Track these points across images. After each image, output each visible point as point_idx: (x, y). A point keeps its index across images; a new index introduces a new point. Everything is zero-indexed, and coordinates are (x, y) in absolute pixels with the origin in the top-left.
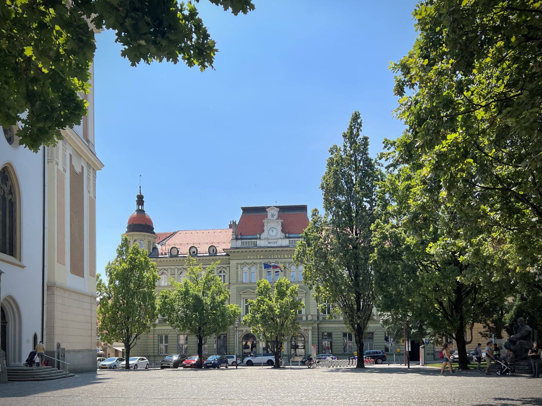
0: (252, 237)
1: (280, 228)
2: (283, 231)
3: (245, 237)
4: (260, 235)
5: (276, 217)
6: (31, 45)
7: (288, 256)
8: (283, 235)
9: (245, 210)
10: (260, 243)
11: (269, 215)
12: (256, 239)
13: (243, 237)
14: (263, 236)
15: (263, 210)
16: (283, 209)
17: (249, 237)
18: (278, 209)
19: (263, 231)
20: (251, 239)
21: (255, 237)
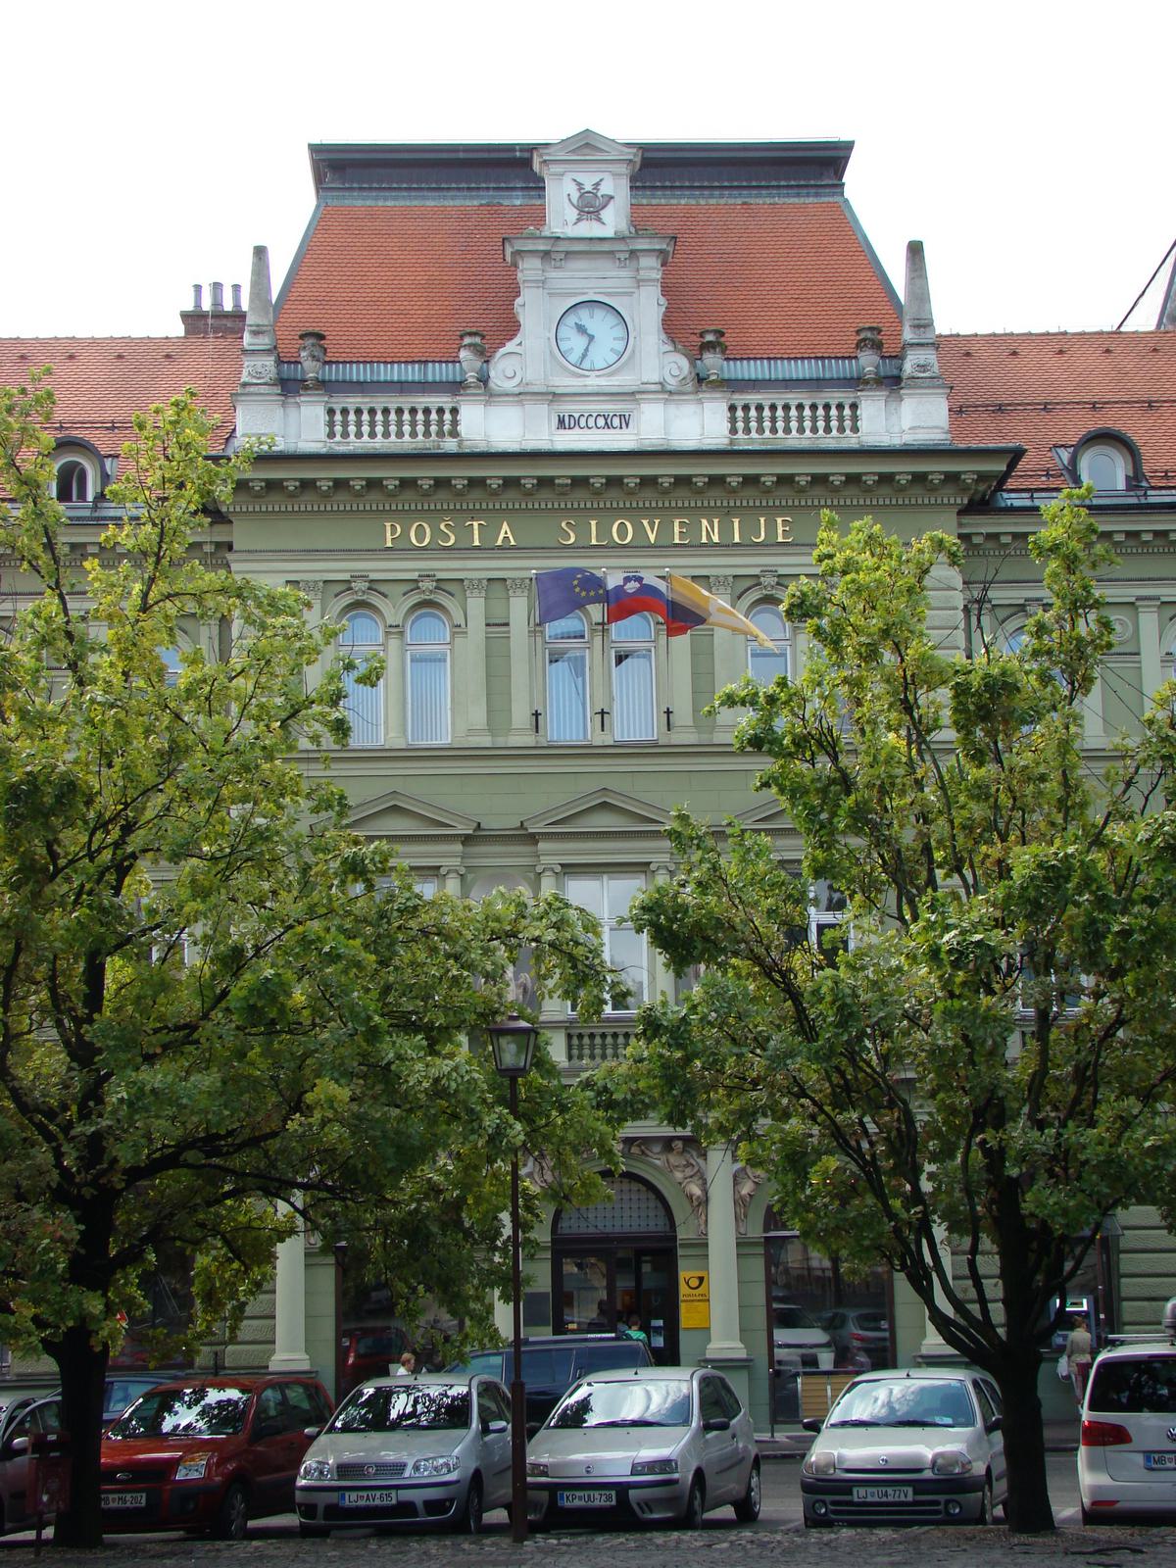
0: (412, 373)
1: (647, 308)
2: (672, 327)
3: (356, 373)
4: (485, 354)
5: (613, 221)
6: (939, 344)
7: (726, 530)
8: (678, 366)
9: (340, 167)
10: (489, 427)
11: (561, 215)
12: (456, 387)
13: (333, 373)
14: (504, 370)
15: (509, 167)
16: (662, 167)
17: (394, 373)
18: (743, 1494)
19: (510, 328)
20: (403, 387)
21: (436, 372)
